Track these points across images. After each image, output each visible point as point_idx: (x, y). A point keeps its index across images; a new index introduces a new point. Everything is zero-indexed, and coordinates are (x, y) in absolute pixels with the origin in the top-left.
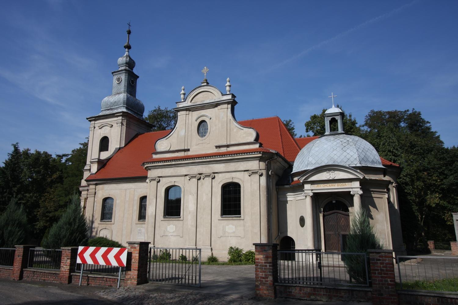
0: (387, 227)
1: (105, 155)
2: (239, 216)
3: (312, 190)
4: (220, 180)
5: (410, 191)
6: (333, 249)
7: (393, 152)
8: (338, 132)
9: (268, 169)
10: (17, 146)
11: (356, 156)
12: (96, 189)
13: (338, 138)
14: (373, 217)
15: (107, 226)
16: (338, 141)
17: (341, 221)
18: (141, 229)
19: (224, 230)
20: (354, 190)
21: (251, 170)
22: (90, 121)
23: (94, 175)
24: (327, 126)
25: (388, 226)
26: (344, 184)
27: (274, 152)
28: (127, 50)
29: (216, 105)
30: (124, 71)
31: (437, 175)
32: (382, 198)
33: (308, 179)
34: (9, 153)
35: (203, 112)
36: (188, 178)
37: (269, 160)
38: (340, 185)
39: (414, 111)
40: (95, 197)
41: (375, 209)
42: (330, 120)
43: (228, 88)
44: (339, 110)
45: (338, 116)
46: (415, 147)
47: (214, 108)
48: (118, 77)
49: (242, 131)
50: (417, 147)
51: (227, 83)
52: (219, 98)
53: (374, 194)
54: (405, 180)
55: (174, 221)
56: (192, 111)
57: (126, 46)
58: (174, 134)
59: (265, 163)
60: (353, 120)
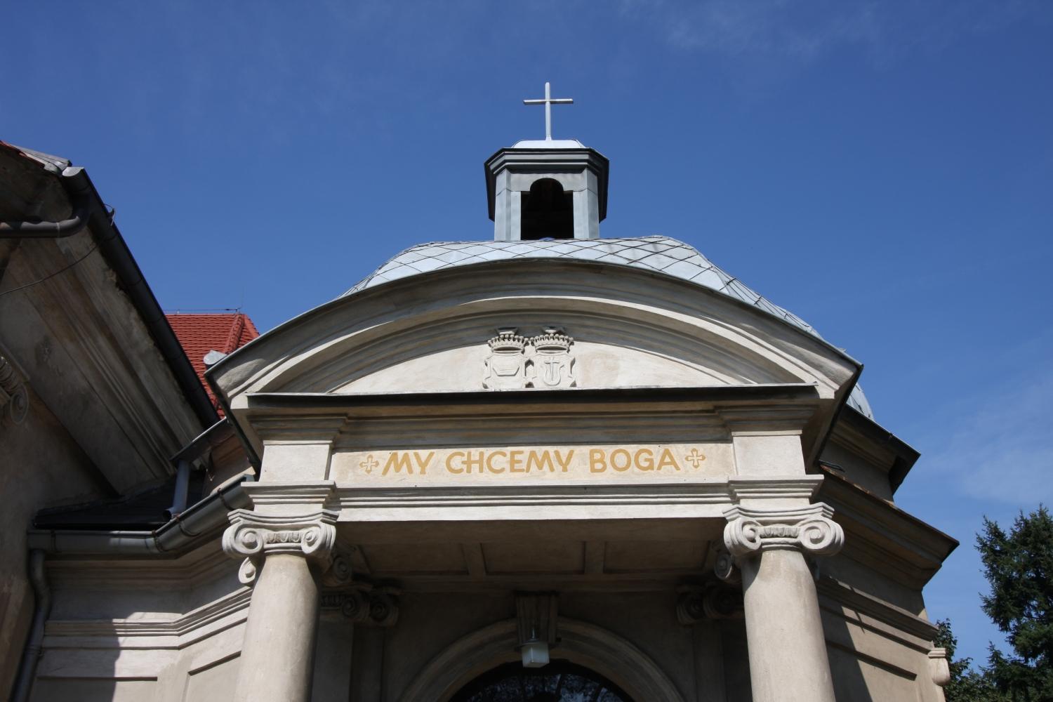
3: (334, 496)
24: (509, 217)
26: (656, 450)
38: (621, 460)
45: (578, 176)
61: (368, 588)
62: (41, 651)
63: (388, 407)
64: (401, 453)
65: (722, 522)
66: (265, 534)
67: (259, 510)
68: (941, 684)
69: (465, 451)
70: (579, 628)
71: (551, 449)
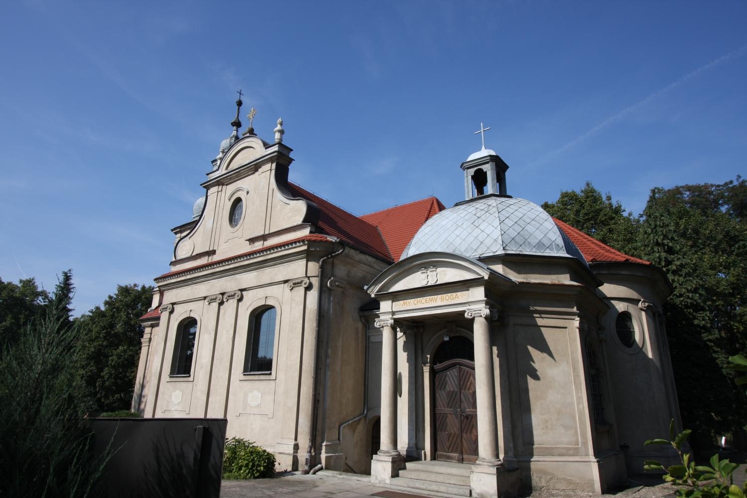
0: (579, 399)
2: (269, 372)
3: (393, 313)
4: (248, 304)
5: (707, 323)
6: (450, 450)
7: (663, 245)
9: (323, 276)
10: (68, 275)
11: (497, 234)
12: (151, 334)
14: (539, 373)
17: (467, 383)
19: (245, 402)
20: (473, 307)
22: (176, 233)
25: (580, 395)
26: (454, 294)
27: (334, 241)
28: (235, 128)
32: (566, 328)
33: (389, 289)
34: (56, 285)
37: (325, 258)
38: (447, 298)
39: (741, 180)
40: (149, 346)
41: (545, 355)
42: (473, 174)
43: (277, 136)
46: (738, 242)
47: (254, 173)
50: (742, 240)
51: (277, 126)
53: (543, 318)
54: (692, 299)
55: (182, 383)
56: (227, 185)
57: (234, 122)
59: (318, 262)
60: (615, 205)
61: (415, 324)
62: (369, 336)
63: (313, 366)
64: (405, 301)
65: (464, 311)
66: (382, 322)
67: (381, 318)
68: (578, 328)
69: (417, 299)
70: (460, 329)
71: (433, 297)
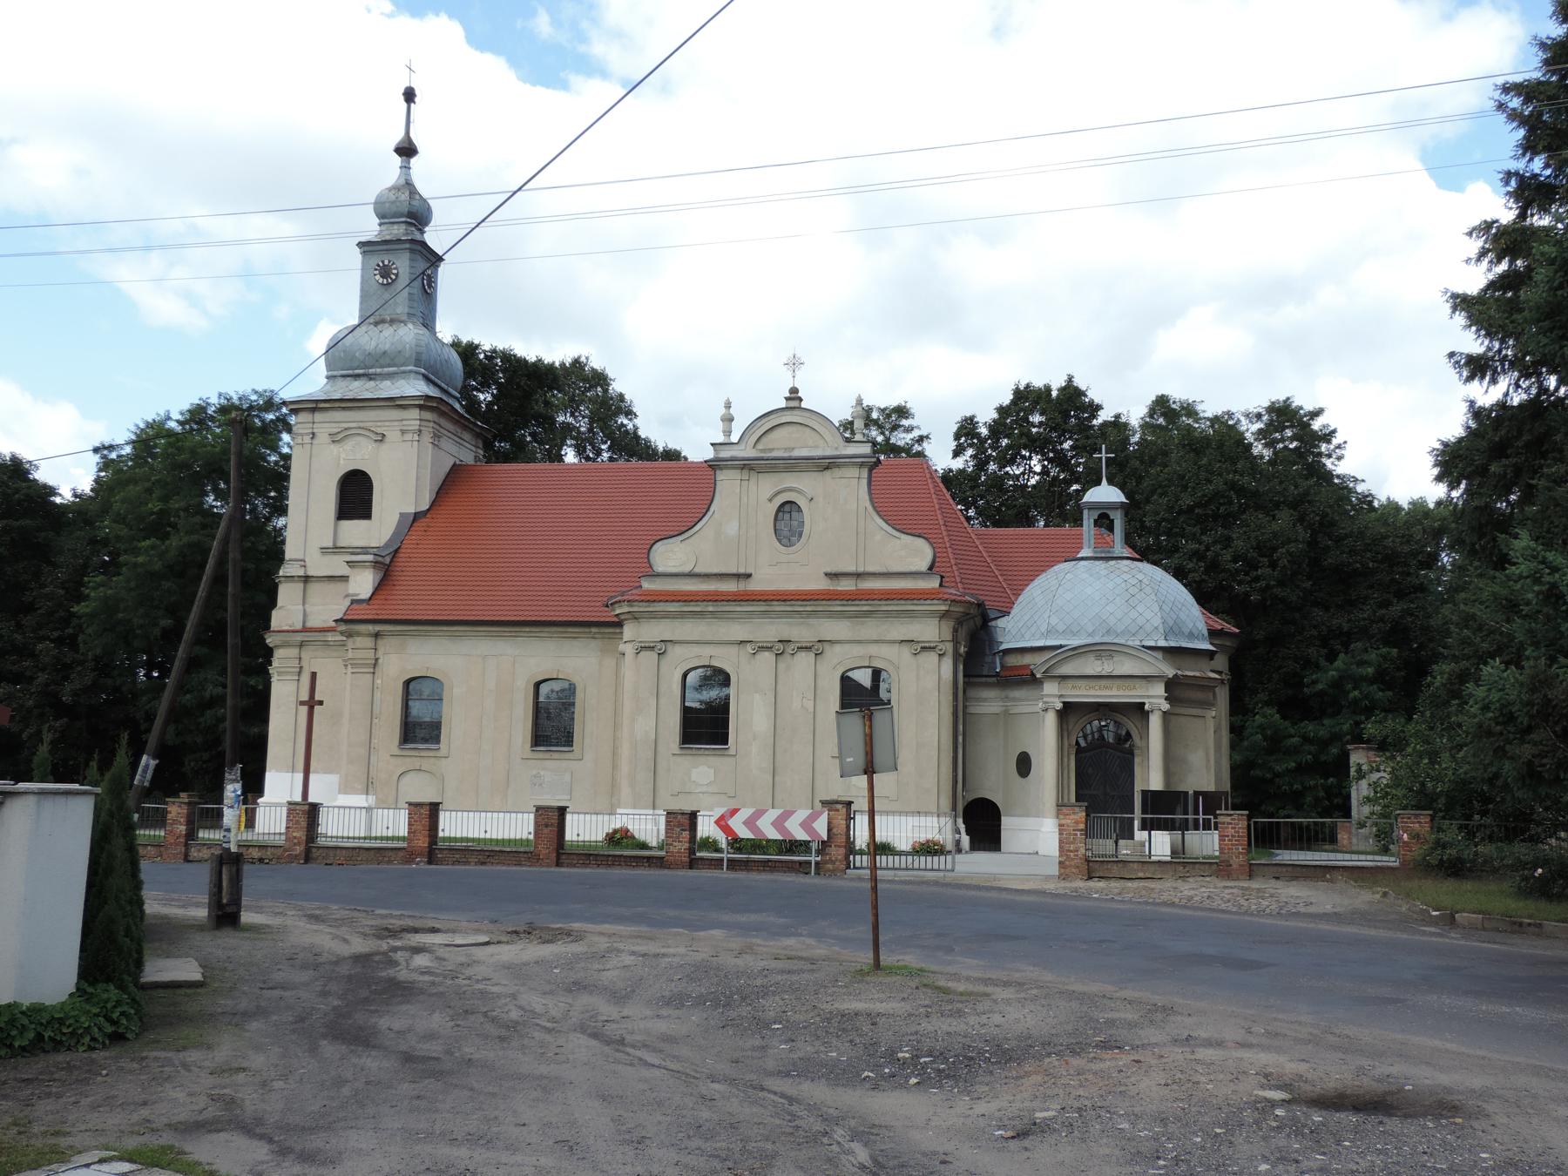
1: (376, 531)
3: (1061, 696)
8: (1114, 552)
11: (1157, 621)
13: (1117, 572)
15: (426, 764)
16: (1118, 580)
18: (542, 773)
21: (918, 642)
23: (364, 606)
29: (828, 464)
30: (407, 246)
31: (1329, 442)
35: (790, 480)
36: (749, 648)
44: (1118, 497)
48: (383, 262)
49: (898, 541)
52: (836, 448)
58: (706, 528)
